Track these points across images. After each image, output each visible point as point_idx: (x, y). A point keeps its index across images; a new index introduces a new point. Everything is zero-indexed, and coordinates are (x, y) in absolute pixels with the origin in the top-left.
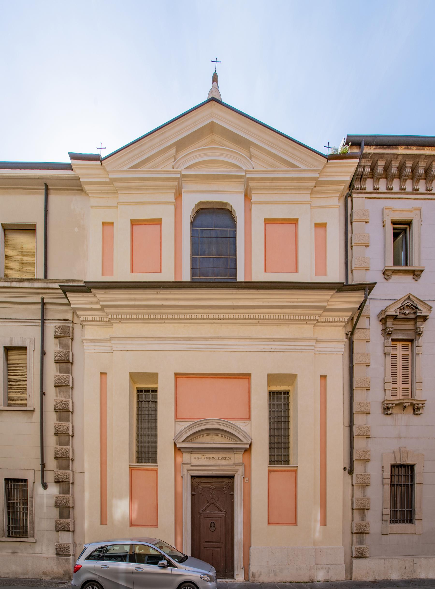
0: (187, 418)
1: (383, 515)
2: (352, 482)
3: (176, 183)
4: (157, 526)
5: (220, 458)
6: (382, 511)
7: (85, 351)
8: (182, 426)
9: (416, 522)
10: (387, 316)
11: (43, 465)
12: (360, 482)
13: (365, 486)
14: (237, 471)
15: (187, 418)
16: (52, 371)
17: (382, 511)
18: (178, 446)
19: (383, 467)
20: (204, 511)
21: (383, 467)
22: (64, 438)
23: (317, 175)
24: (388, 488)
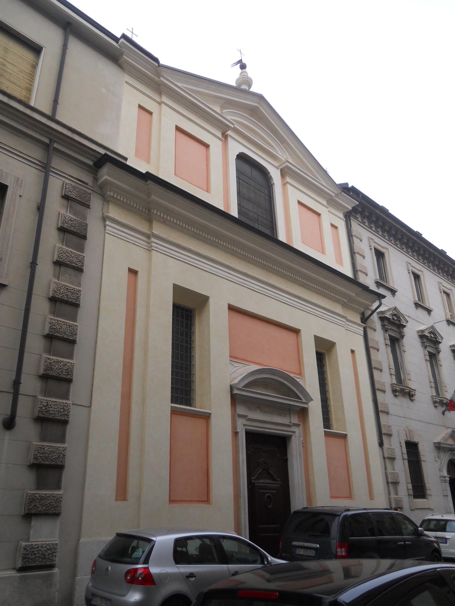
0: (240, 359)
1: (408, 489)
2: (383, 455)
3: (387, 460)
4: (207, 501)
5: (66, 282)
6: (407, 486)
7: (107, 231)
8: (236, 367)
9: (429, 497)
10: (385, 317)
11: (17, 383)
12: (390, 456)
13: (392, 459)
14: (294, 432)
15: (240, 359)
16: (51, 240)
17: (407, 486)
18: (236, 392)
19: (400, 443)
20: (255, 480)
21: (400, 443)
22: (58, 345)
23: (334, 195)
24: (406, 462)
